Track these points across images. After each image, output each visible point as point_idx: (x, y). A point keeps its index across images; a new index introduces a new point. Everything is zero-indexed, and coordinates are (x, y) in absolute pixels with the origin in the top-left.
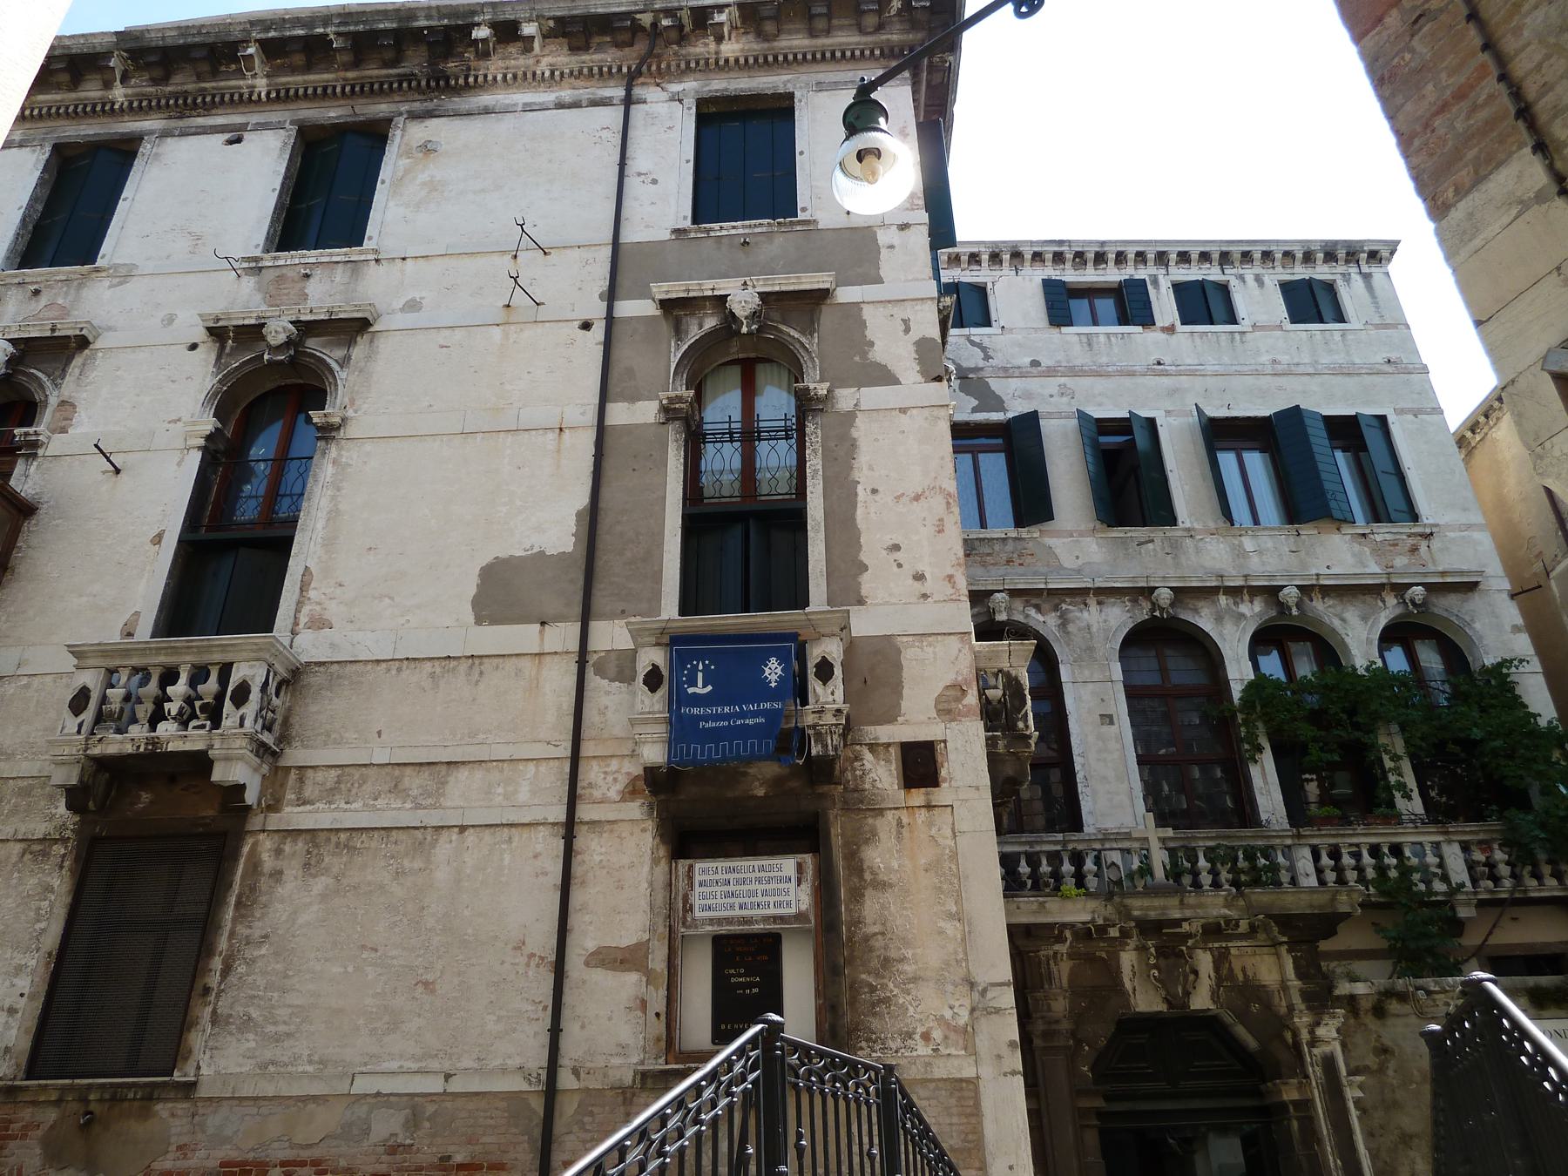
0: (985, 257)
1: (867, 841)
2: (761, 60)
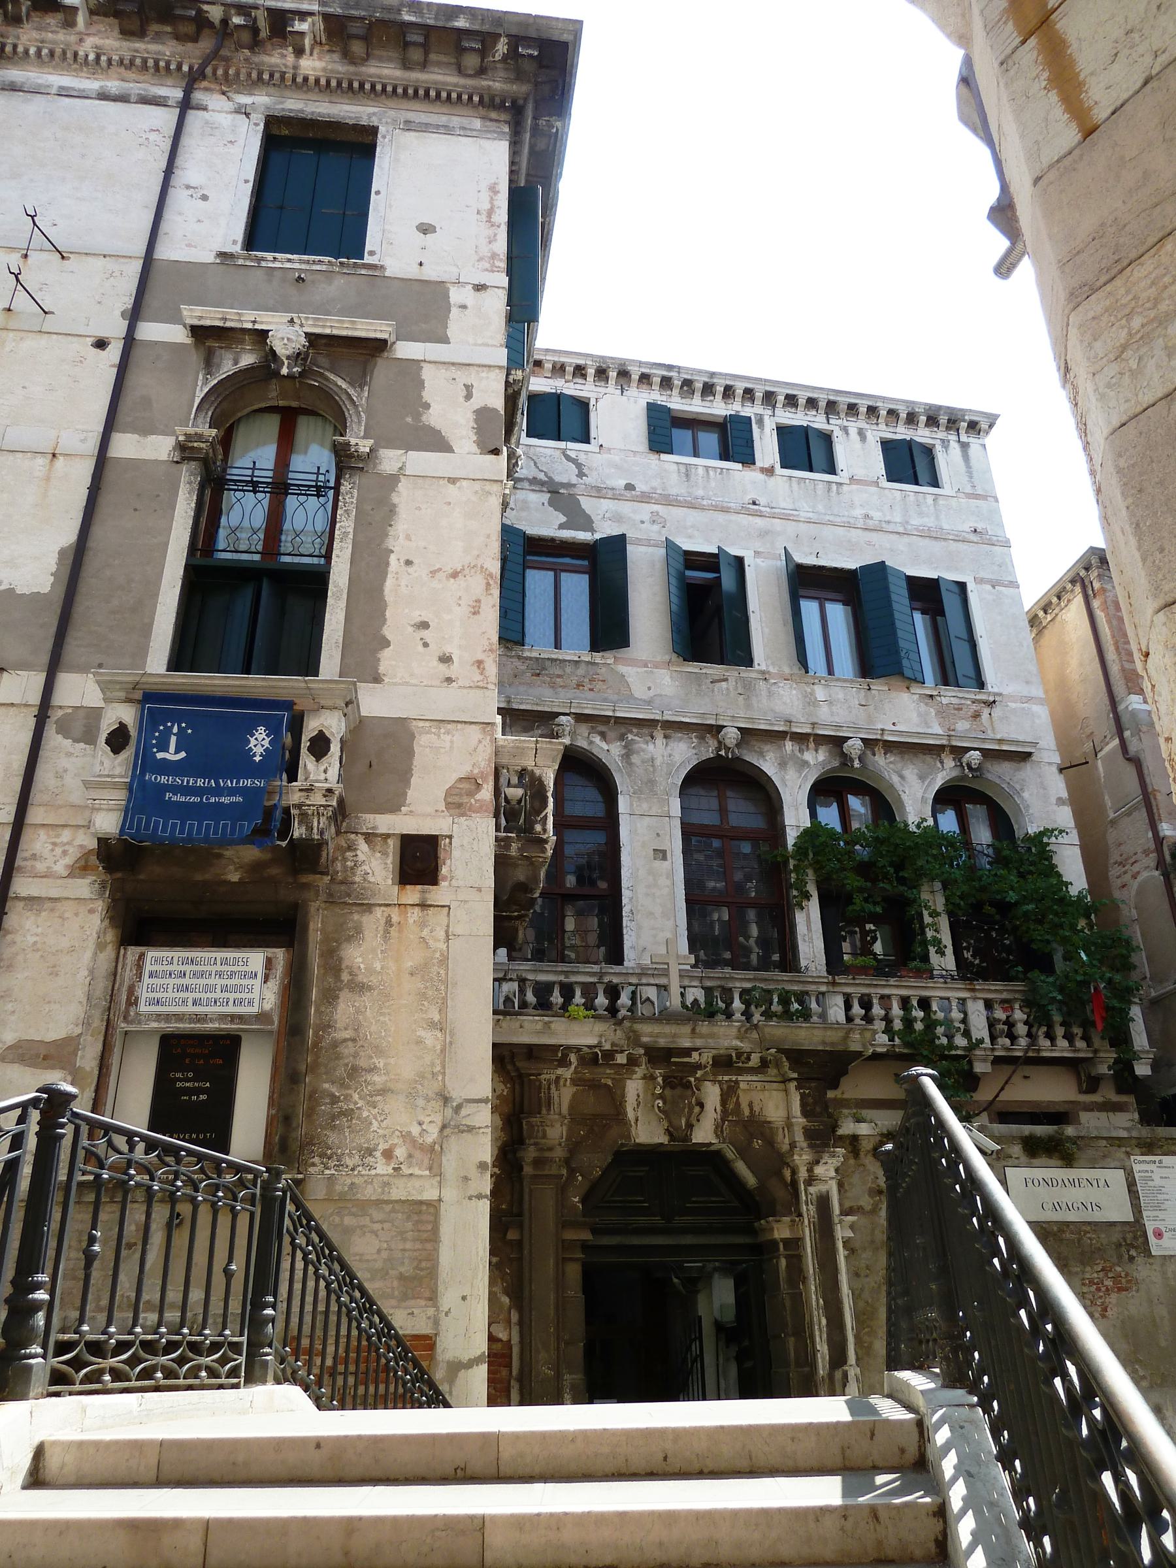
0: (591, 372)
1: (349, 939)
2: (345, 85)
